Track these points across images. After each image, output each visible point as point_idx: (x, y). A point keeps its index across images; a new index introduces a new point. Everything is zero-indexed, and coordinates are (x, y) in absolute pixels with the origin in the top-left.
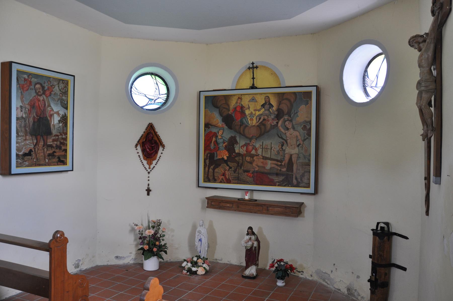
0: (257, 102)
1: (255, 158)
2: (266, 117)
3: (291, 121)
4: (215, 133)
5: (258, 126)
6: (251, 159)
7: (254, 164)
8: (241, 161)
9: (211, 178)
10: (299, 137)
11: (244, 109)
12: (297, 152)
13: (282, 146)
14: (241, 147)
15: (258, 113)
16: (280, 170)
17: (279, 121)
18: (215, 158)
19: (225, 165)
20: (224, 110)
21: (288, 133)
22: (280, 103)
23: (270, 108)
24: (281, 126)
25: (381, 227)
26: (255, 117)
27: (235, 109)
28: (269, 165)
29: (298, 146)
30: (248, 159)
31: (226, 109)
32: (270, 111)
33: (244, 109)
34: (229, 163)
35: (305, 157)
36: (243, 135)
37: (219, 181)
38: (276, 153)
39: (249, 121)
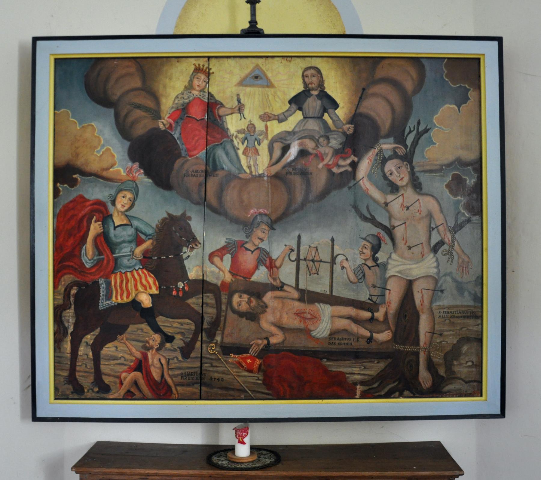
0: (270, 85)
2: (310, 145)
4: (99, 203)
5: (277, 176)
9: (86, 381)
11: (222, 111)
14: (212, 256)
15: (276, 128)
18: (103, 304)
19: (145, 326)
22: (361, 95)
23: (325, 110)
27: (183, 112)
32: (325, 123)
33: (222, 111)
34: (161, 320)
35: (460, 288)
37: (122, 391)
39: (243, 158)
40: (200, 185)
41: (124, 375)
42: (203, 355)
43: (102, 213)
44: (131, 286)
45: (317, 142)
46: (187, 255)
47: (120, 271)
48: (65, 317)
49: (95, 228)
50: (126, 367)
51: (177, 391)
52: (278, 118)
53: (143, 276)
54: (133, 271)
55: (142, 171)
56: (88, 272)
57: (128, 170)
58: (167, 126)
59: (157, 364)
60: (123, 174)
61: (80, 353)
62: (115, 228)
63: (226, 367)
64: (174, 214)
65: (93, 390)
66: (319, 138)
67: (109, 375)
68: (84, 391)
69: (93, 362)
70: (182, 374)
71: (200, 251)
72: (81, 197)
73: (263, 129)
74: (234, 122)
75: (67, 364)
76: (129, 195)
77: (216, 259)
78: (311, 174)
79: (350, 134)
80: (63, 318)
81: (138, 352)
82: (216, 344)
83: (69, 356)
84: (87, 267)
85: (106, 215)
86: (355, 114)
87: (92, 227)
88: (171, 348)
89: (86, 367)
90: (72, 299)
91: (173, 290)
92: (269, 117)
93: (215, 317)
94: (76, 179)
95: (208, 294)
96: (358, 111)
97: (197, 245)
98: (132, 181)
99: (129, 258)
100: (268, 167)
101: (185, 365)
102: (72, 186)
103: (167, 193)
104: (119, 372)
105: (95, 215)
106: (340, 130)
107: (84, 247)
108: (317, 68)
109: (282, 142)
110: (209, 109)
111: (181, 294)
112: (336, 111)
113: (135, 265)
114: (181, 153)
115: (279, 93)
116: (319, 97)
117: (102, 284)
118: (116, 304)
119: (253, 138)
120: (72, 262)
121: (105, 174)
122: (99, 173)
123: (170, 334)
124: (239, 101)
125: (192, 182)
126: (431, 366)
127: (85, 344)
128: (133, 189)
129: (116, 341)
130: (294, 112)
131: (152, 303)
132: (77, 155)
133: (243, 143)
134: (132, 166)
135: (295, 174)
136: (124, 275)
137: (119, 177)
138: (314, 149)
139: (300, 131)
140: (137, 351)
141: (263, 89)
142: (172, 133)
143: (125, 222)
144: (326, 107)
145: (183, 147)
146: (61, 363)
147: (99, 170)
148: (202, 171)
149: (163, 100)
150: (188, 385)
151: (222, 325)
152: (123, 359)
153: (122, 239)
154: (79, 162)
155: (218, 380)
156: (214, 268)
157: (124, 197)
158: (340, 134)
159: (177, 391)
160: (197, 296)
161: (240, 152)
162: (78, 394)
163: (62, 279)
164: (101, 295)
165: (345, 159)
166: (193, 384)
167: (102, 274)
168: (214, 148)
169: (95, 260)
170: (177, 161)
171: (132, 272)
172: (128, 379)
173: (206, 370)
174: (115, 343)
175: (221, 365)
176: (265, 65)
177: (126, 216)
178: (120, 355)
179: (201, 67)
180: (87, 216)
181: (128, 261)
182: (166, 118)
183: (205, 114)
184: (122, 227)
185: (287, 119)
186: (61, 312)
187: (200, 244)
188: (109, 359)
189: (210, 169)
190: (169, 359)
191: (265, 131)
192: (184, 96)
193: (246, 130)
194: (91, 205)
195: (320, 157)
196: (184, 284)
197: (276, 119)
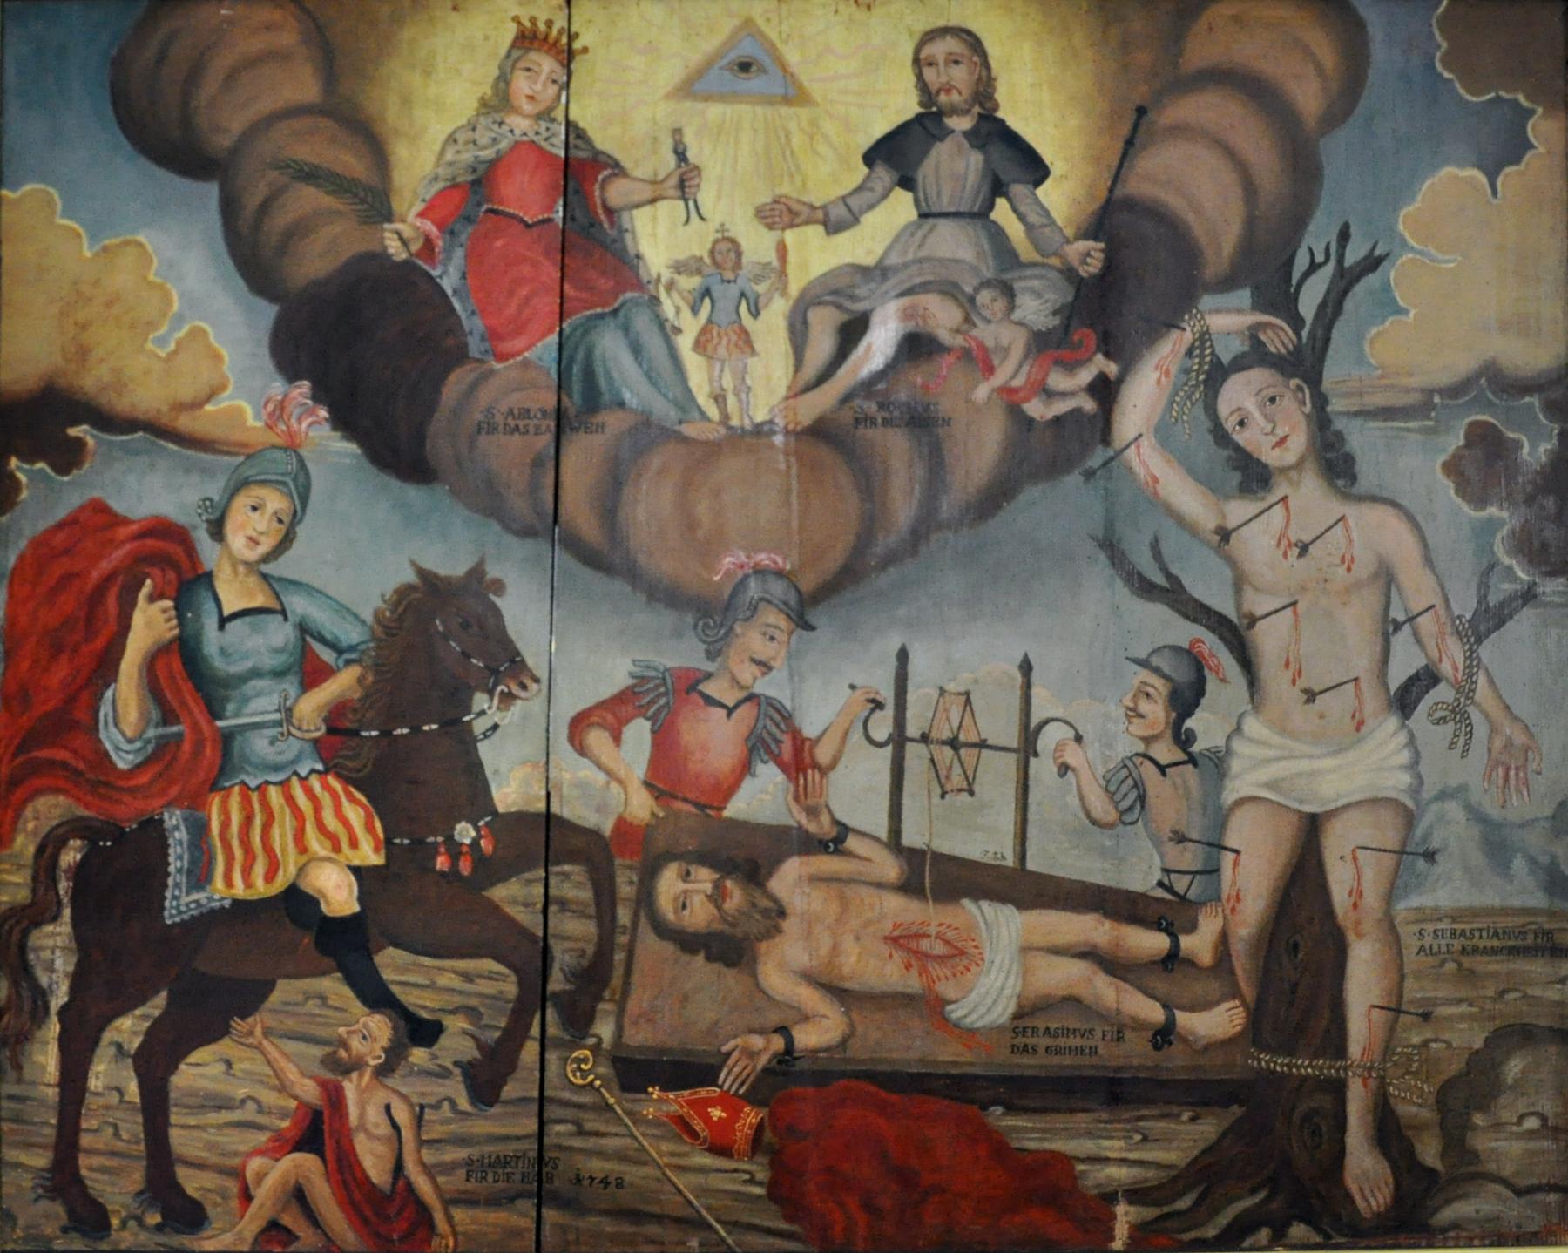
0: (794, 94)
1: (789, 879)
2: (942, 317)
3: (1304, 366)
4: (164, 530)
5: (820, 431)
6: (736, 896)
7: (781, 969)
8: (574, 933)
10: (1417, 588)
11: (617, 193)
12: (1397, 782)
13: (1186, 699)
14: (579, 724)
15: (817, 255)
16: (1164, 1035)
17: (1128, 364)
19: (334, 986)
20: (307, 199)
21: (1260, 535)
23: (998, 188)
24: (1164, 433)
25: (554, 1225)
26: (777, 312)
27: (472, 194)
28: (1003, 968)
29: (1404, 701)
30: (687, 894)
31: (338, 184)
32: (997, 235)
33: (617, 193)
34: (392, 964)
36: (598, 556)
38: (1100, 806)
39: (694, 364)
40: (537, 463)
41: (255, 1164)
42: (548, 1093)
45: (969, 304)
46: (490, 724)
47: (243, 783)
48: (36, 950)
49: (149, 624)
50: (263, 1138)
51: (452, 1226)
52: (826, 215)
53: (326, 800)
55: (323, 413)
57: (270, 407)
58: (415, 247)
59: (377, 1125)
60: (251, 422)
61: (94, 1084)
62: (223, 622)
63: (632, 1135)
64: (442, 572)
65: (140, 1221)
66: (977, 290)
67: (201, 1166)
69: (140, 1119)
70: (469, 1163)
72: (99, 507)
73: (772, 257)
74: (661, 230)
75: (46, 1124)
76: (275, 502)
77: (597, 739)
78: (947, 422)
79: (1092, 276)
80: (31, 956)
81: (306, 1081)
82: (596, 1049)
83: (52, 1093)
84: (121, 765)
86: (1108, 201)
87: (138, 619)
88: (431, 1066)
89: (116, 1134)
90: (64, 886)
91: (437, 853)
92: (793, 213)
93: (590, 950)
94: (79, 443)
95: (567, 868)
96: (1118, 192)
97: (524, 687)
98: (284, 449)
99: (274, 732)
100: (787, 398)
101: (481, 1126)
102: (63, 468)
104: (236, 1154)
105: (148, 575)
106: (1055, 261)
108: (969, 33)
109: (839, 307)
110: (571, 184)
111: (465, 867)
112: (1040, 192)
114: (466, 345)
115: (829, 127)
116: (974, 137)
117: (177, 828)
118: (227, 903)
119: (734, 290)
120: (65, 748)
121: (184, 423)
122: (165, 420)
123: (425, 1015)
124: (681, 155)
125: (508, 455)
126: (1389, 1133)
127: (113, 1050)
128: (288, 480)
129: (226, 1041)
130: (885, 196)
131: (360, 899)
132: (83, 353)
133: (695, 310)
134: (286, 395)
135: (886, 422)
136: (255, 797)
137: (237, 436)
138: (958, 331)
139: (906, 265)
140: (303, 1075)
141: (769, 111)
142: (435, 273)
143: (260, 601)
144: (1004, 178)
145: (473, 325)
146: (24, 1122)
147: (165, 408)
148: (544, 413)
149: (401, 152)
150: (493, 1202)
152: (251, 1105)
154: (91, 381)
155: (605, 1182)
156: (586, 771)
157: (254, 509)
158: (1054, 275)
159: (452, 1226)
160: (527, 875)
161: (685, 343)
162: (84, 1234)
163: (29, 812)
164: (172, 869)
165: (1070, 367)
166: (512, 1200)
167: (174, 791)
168: (588, 327)
169: (148, 741)
170: (453, 377)
171: (284, 785)
172: (269, 1182)
173: (560, 1147)
174: (224, 1047)
175: (613, 1130)
176: (775, 21)
177: (265, 577)
178: (241, 1092)
179: (542, 27)
180: (121, 579)
181: (272, 743)
182: (411, 217)
183: (555, 202)
184: (247, 619)
185: (856, 221)
186: (25, 934)
187: (537, 680)
188: (202, 1108)
189: (574, 402)
190: (422, 1107)
191: (775, 263)
192: (477, 135)
193: (707, 260)
195: (981, 361)
196: (477, 829)
197: (816, 222)
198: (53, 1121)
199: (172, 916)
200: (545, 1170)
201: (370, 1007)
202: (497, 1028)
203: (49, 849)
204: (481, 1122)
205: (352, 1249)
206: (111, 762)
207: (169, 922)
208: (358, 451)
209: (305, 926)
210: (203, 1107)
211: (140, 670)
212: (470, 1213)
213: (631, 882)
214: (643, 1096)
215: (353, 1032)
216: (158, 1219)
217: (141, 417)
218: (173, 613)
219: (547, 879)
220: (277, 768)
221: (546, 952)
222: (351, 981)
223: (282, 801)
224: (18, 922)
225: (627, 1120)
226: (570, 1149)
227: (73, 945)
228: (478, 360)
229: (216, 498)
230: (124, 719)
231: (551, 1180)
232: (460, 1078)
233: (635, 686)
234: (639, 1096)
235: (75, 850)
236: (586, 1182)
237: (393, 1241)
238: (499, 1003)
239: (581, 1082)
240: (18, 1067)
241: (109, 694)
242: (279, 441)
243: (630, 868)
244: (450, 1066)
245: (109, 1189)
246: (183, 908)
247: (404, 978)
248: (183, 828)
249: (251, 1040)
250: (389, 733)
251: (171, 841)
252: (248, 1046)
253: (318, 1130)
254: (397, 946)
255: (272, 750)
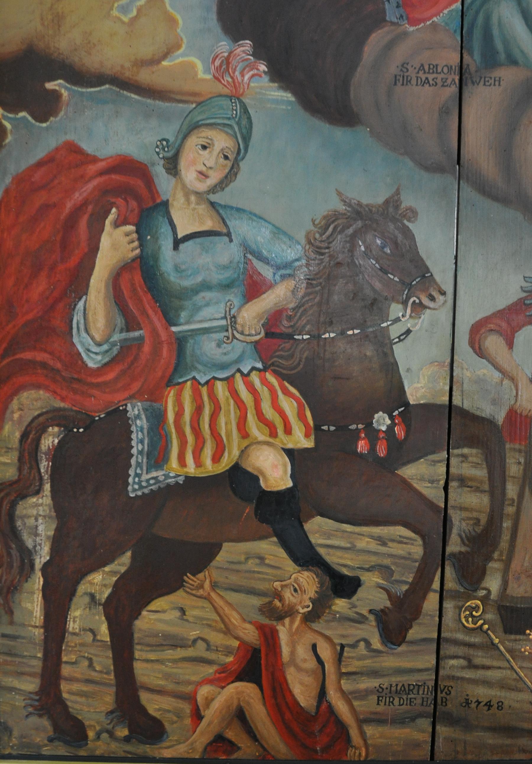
4: (126, 166)
14: (477, 330)
18: (141, 479)
19: (271, 549)
34: (319, 530)
40: (444, 111)
41: (204, 691)
42: (443, 635)
43: (138, 198)
44: (227, 423)
46: (404, 330)
47: (194, 378)
48: (23, 517)
49: (114, 247)
50: (211, 670)
51: (365, 740)
53: (264, 393)
54: (233, 376)
55: (263, 67)
56: (94, 380)
57: (217, 63)
59: (305, 661)
60: (201, 75)
61: (72, 626)
62: (177, 243)
63: (512, 668)
64: (365, 201)
65: (111, 734)
67: (160, 692)
68: (86, 737)
69: (110, 654)
70: (379, 690)
71: (444, 316)
72: (72, 148)
75: (35, 657)
76: (222, 141)
80: (19, 523)
81: (248, 626)
82: (485, 600)
83: (38, 633)
84: (91, 364)
85: (151, 204)
87: (105, 241)
88: (351, 614)
89: (91, 665)
90: (44, 465)
91: (358, 438)
93: (484, 519)
94: (56, 95)
95: (466, 451)
97: (432, 298)
98: (230, 97)
99: (221, 336)
101: (390, 662)
102: (42, 118)
103: (340, 134)
104: (189, 683)
105: (112, 205)
107: (81, 304)
111: (382, 451)
113: (238, 360)
117: (138, 417)
118: (181, 480)
120: (45, 351)
121: (145, 76)
122: (127, 74)
123: (345, 571)
125: (422, 102)
127: (87, 599)
128: (232, 122)
129: (180, 593)
131: (292, 476)
132: (58, 20)
134: (230, 53)
136: (204, 391)
137: (188, 87)
140: (244, 620)
143: (208, 225)
146: (16, 655)
147: (127, 65)
148: (450, 68)
150: (400, 721)
151: (504, 544)
152: (201, 645)
153: (199, 279)
154: (64, 43)
155: (489, 705)
156: (484, 370)
157: (204, 147)
159: (365, 740)
160: (431, 457)
162: (67, 743)
163: (15, 404)
164: (134, 451)
166: (413, 719)
167: (136, 386)
169: (114, 344)
171: (229, 380)
172: (216, 705)
173: (453, 678)
174: (179, 597)
175: (495, 663)
177: (213, 205)
178: (194, 634)
180: (90, 208)
181: (219, 346)
184: (198, 240)
186: (13, 505)
187: (443, 293)
188: (160, 646)
189: (474, 60)
190: (342, 647)
194: (101, 173)
196: (391, 417)
198: (40, 655)
199: (134, 490)
200: (439, 695)
201: (300, 565)
202: (405, 582)
203: (31, 436)
204: (391, 658)
205: (283, 757)
206: (83, 362)
207: (132, 495)
208: (293, 99)
209: (246, 499)
210: (162, 645)
211: (107, 286)
212: (380, 729)
213: (519, 463)
214: (521, 637)
215: (286, 586)
216: (125, 732)
217: (108, 72)
218: (135, 236)
219: (448, 459)
220: (223, 367)
221: (446, 519)
222: (284, 544)
223: (227, 393)
224: (7, 495)
225: (507, 655)
226: (462, 679)
227: (54, 514)
228: (393, 23)
229: (172, 139)
230: (94, 327)
231: (445, 702)
232: (374, 623)
233: (526, 298)
234: (518, 637)
235: (54, 435)
236: (473, 705)
237: (316, 751)
238: (408, 562)
239: (471, 626)
240: (10, 612)
241: (81, 305)
242: (226, 91)
243: (520, 451)
244: (365, 612)
245: (86, 709)
246: (144, 484)
247: (329, 542)
248: (143, 416)
249: (201, 592)
250: (319, 336)
251: (133, 428)
252: (200, 597)
253: (257, 664)
254: (322, 515)
255: (220, 351)
